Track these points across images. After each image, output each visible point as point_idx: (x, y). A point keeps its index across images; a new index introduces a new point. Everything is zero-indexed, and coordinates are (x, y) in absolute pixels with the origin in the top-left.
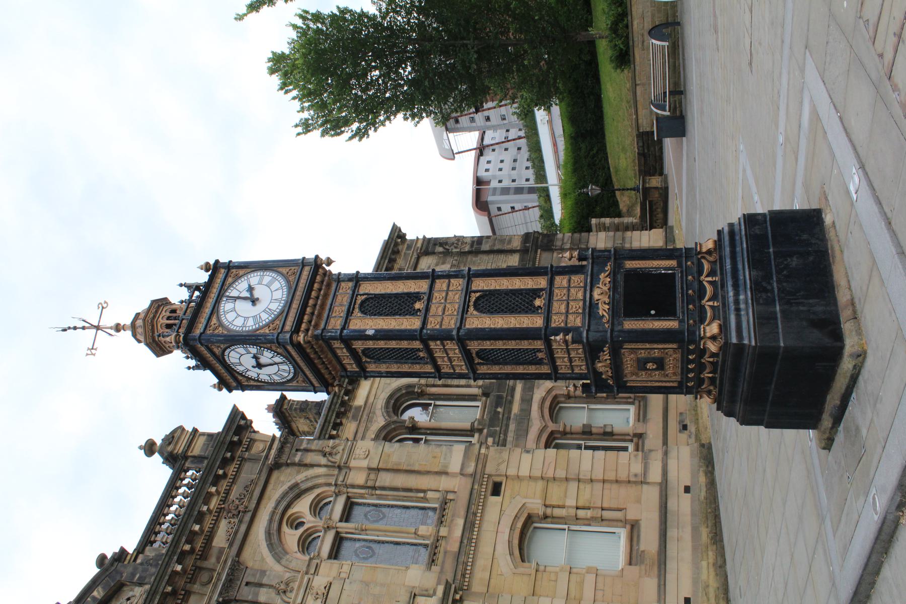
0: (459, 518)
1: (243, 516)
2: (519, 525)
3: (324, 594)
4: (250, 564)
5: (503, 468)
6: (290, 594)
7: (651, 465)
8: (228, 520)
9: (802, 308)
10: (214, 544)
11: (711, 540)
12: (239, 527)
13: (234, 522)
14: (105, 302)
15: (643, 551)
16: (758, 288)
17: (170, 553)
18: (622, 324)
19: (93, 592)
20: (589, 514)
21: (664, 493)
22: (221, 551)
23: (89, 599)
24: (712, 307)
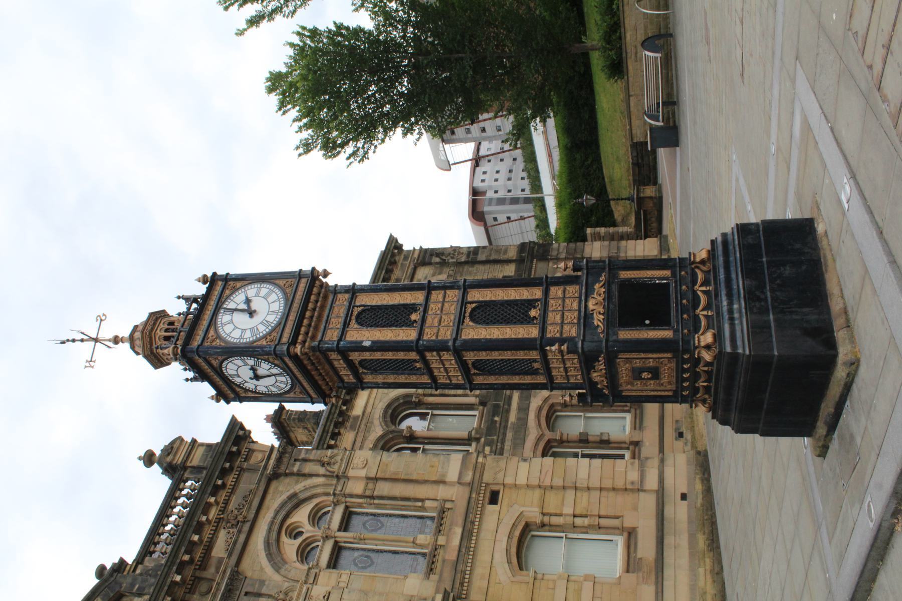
1: (242, 526)
4: (249, 574)
5: (500, 476)
8: (227, 531)
10: (213, 554)
12: (238, 537)
14: (104, 315)
15: (641, 559)
16: (752, 297)
18: (617, 334)
20: (586, 521)
22: (220, 561)
24: (706, 316)
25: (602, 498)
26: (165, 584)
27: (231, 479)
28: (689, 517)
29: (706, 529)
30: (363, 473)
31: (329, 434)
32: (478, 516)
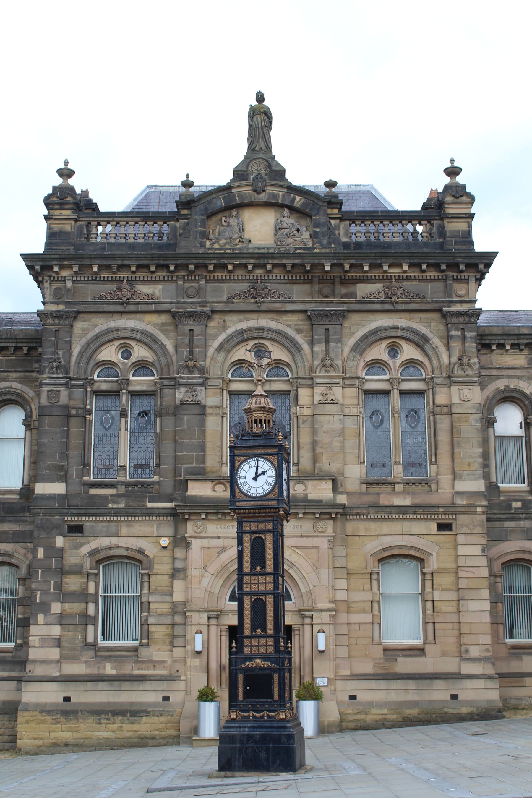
0: (412, 499)
1: (388, 303)
2: (412, 553)
3: (327, 400)
4: (346, 325)
5: (466, 530)
6: (324, 371)
7: (478, 664)
9: (237, 755)
10: (358, 285)
11: (407, 717)
12: (377, 302)
13: (380, 296)
15: (396, 660)
16: (249, 737)
17: (337, 255)
18: (241, 673)
19: (298, 195)
20: (429, 612)
21: (449, 676)
22: (353, 295)
23: (292, 195)
24: (249, 716)
25: (452, 624)
26: (319, 259)
27: (432, 274)
28: (434, 701)
29: (423, 716)
30: (455, 400)
31: (516, 342)
32: (422, 517)
